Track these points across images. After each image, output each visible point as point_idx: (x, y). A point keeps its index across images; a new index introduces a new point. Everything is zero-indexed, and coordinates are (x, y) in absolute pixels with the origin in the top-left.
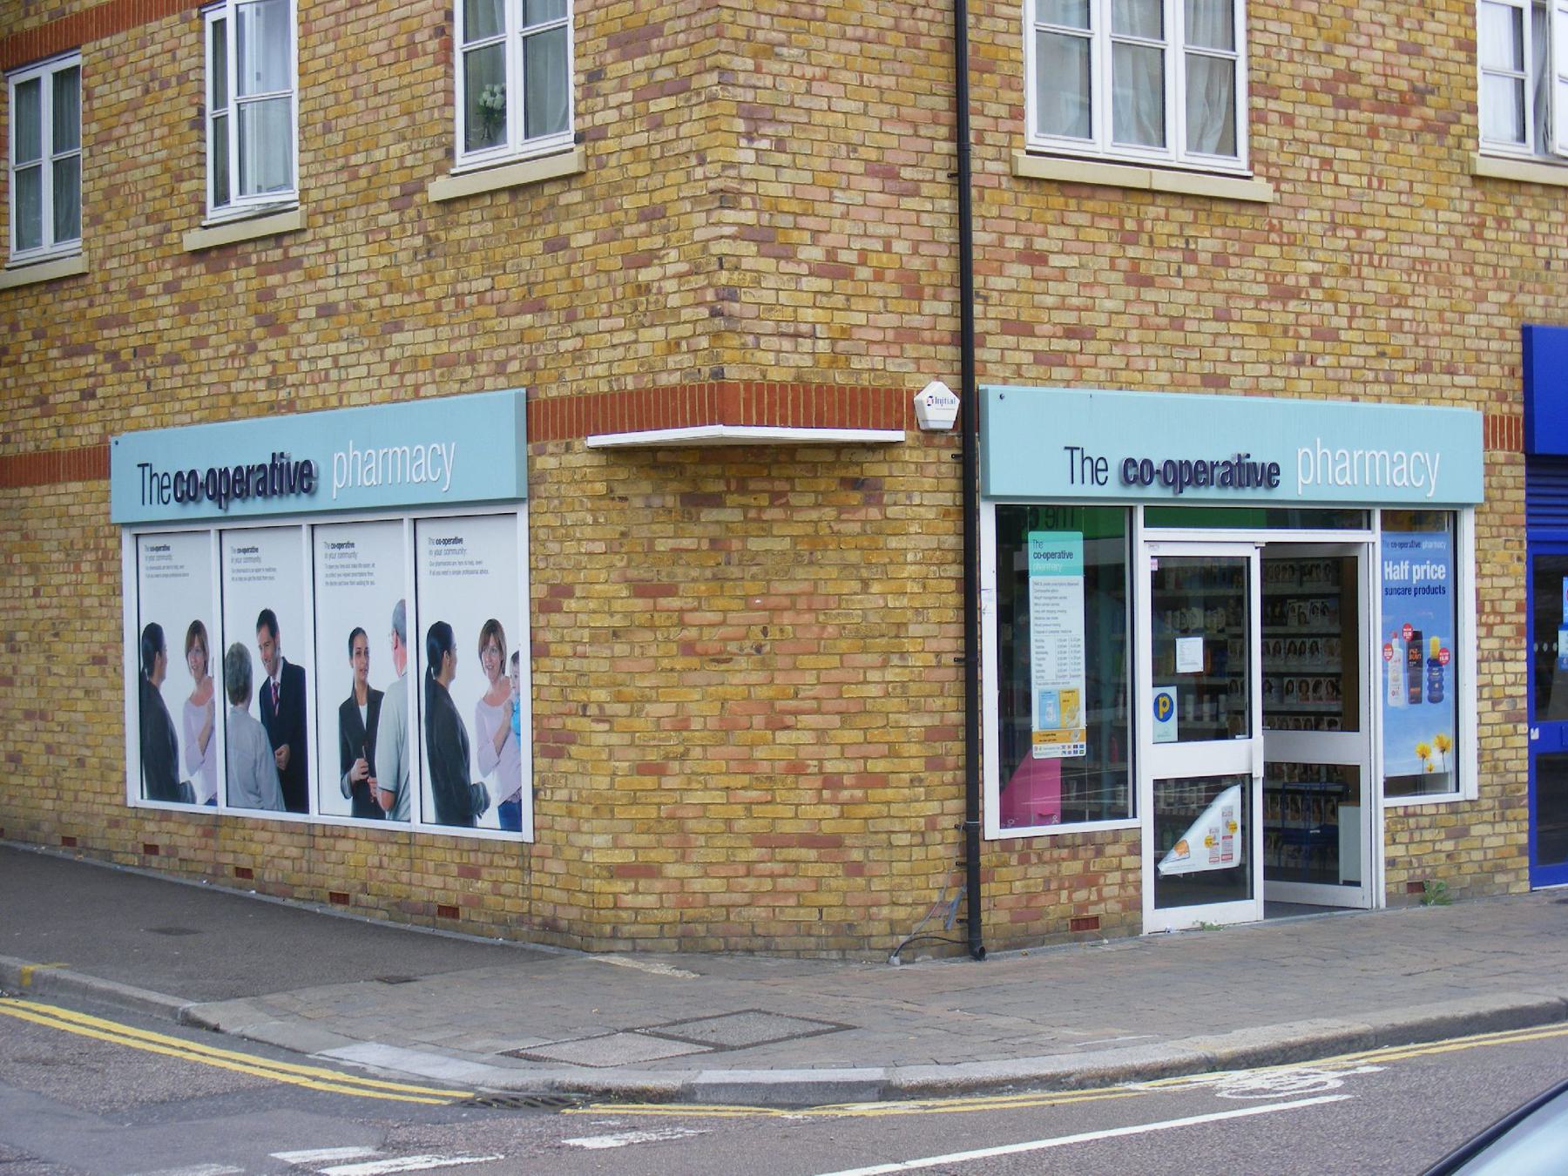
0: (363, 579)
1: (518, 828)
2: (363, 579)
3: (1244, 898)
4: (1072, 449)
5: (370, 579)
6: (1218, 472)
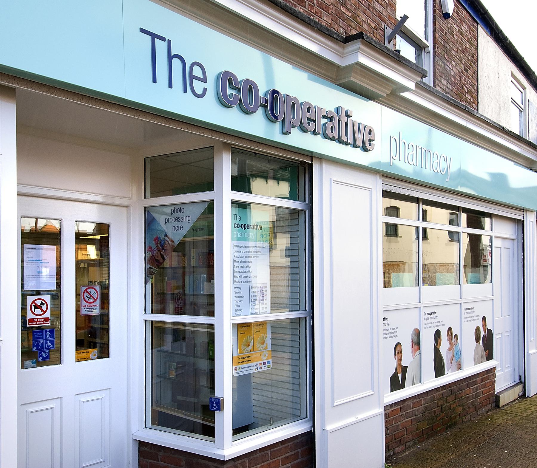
0: (392, 335)
2: (392, 335)
3: (212, 191)
4: (154, 36)
5: (395, 334)
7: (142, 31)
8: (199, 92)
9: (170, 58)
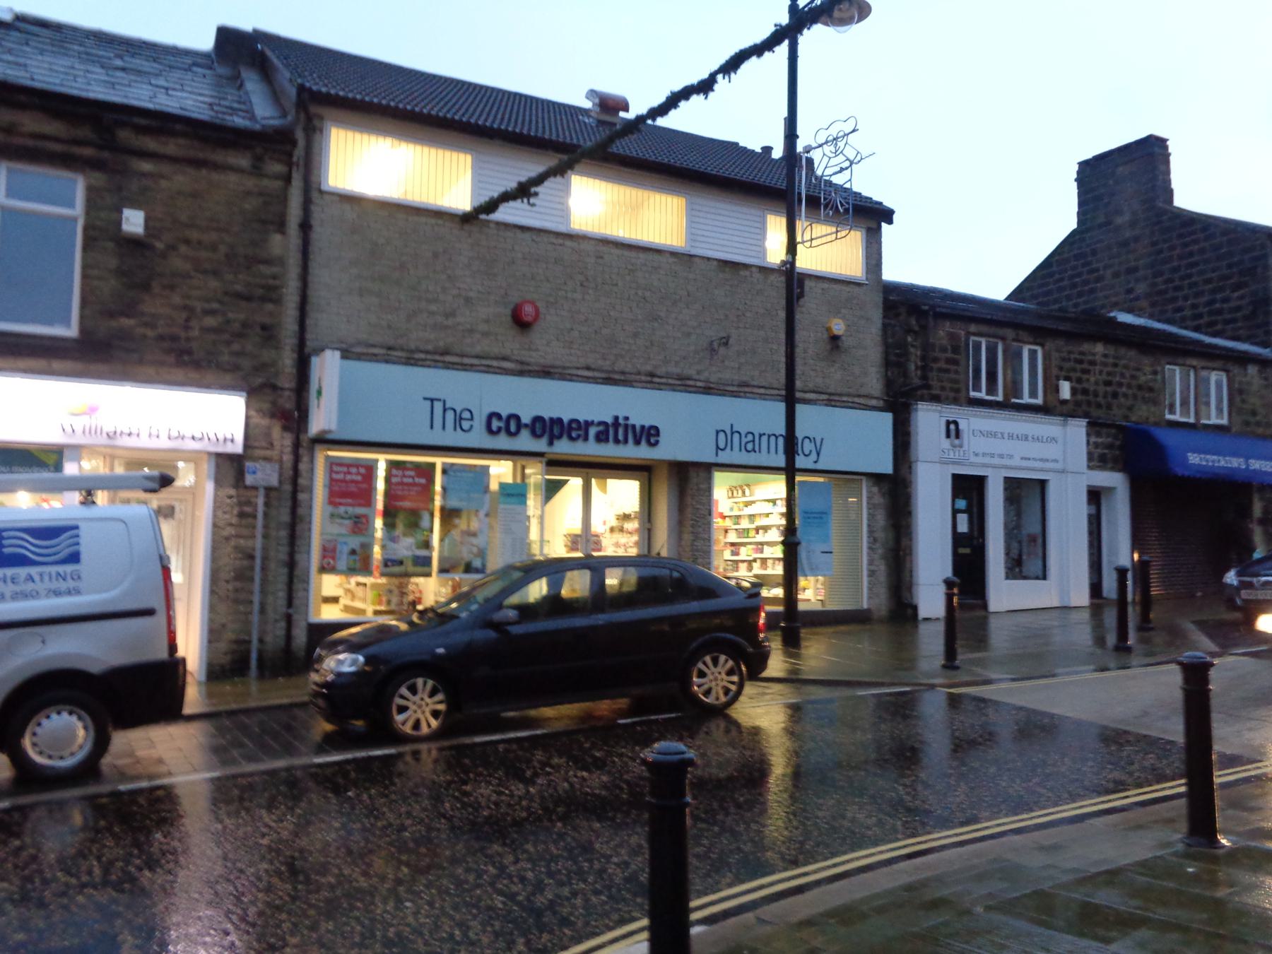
1: (980, 391)
4: (432, 400)
6: (593, 431)
7: (425, 399)
8: (494, 428)
9: (445, 410)
